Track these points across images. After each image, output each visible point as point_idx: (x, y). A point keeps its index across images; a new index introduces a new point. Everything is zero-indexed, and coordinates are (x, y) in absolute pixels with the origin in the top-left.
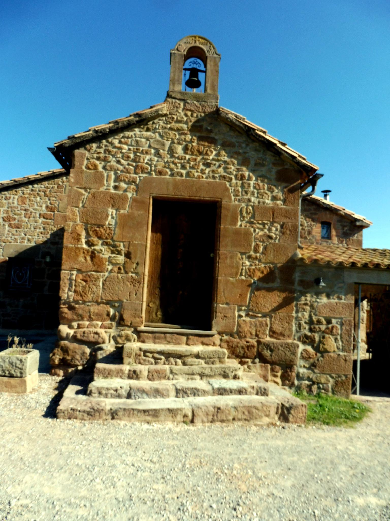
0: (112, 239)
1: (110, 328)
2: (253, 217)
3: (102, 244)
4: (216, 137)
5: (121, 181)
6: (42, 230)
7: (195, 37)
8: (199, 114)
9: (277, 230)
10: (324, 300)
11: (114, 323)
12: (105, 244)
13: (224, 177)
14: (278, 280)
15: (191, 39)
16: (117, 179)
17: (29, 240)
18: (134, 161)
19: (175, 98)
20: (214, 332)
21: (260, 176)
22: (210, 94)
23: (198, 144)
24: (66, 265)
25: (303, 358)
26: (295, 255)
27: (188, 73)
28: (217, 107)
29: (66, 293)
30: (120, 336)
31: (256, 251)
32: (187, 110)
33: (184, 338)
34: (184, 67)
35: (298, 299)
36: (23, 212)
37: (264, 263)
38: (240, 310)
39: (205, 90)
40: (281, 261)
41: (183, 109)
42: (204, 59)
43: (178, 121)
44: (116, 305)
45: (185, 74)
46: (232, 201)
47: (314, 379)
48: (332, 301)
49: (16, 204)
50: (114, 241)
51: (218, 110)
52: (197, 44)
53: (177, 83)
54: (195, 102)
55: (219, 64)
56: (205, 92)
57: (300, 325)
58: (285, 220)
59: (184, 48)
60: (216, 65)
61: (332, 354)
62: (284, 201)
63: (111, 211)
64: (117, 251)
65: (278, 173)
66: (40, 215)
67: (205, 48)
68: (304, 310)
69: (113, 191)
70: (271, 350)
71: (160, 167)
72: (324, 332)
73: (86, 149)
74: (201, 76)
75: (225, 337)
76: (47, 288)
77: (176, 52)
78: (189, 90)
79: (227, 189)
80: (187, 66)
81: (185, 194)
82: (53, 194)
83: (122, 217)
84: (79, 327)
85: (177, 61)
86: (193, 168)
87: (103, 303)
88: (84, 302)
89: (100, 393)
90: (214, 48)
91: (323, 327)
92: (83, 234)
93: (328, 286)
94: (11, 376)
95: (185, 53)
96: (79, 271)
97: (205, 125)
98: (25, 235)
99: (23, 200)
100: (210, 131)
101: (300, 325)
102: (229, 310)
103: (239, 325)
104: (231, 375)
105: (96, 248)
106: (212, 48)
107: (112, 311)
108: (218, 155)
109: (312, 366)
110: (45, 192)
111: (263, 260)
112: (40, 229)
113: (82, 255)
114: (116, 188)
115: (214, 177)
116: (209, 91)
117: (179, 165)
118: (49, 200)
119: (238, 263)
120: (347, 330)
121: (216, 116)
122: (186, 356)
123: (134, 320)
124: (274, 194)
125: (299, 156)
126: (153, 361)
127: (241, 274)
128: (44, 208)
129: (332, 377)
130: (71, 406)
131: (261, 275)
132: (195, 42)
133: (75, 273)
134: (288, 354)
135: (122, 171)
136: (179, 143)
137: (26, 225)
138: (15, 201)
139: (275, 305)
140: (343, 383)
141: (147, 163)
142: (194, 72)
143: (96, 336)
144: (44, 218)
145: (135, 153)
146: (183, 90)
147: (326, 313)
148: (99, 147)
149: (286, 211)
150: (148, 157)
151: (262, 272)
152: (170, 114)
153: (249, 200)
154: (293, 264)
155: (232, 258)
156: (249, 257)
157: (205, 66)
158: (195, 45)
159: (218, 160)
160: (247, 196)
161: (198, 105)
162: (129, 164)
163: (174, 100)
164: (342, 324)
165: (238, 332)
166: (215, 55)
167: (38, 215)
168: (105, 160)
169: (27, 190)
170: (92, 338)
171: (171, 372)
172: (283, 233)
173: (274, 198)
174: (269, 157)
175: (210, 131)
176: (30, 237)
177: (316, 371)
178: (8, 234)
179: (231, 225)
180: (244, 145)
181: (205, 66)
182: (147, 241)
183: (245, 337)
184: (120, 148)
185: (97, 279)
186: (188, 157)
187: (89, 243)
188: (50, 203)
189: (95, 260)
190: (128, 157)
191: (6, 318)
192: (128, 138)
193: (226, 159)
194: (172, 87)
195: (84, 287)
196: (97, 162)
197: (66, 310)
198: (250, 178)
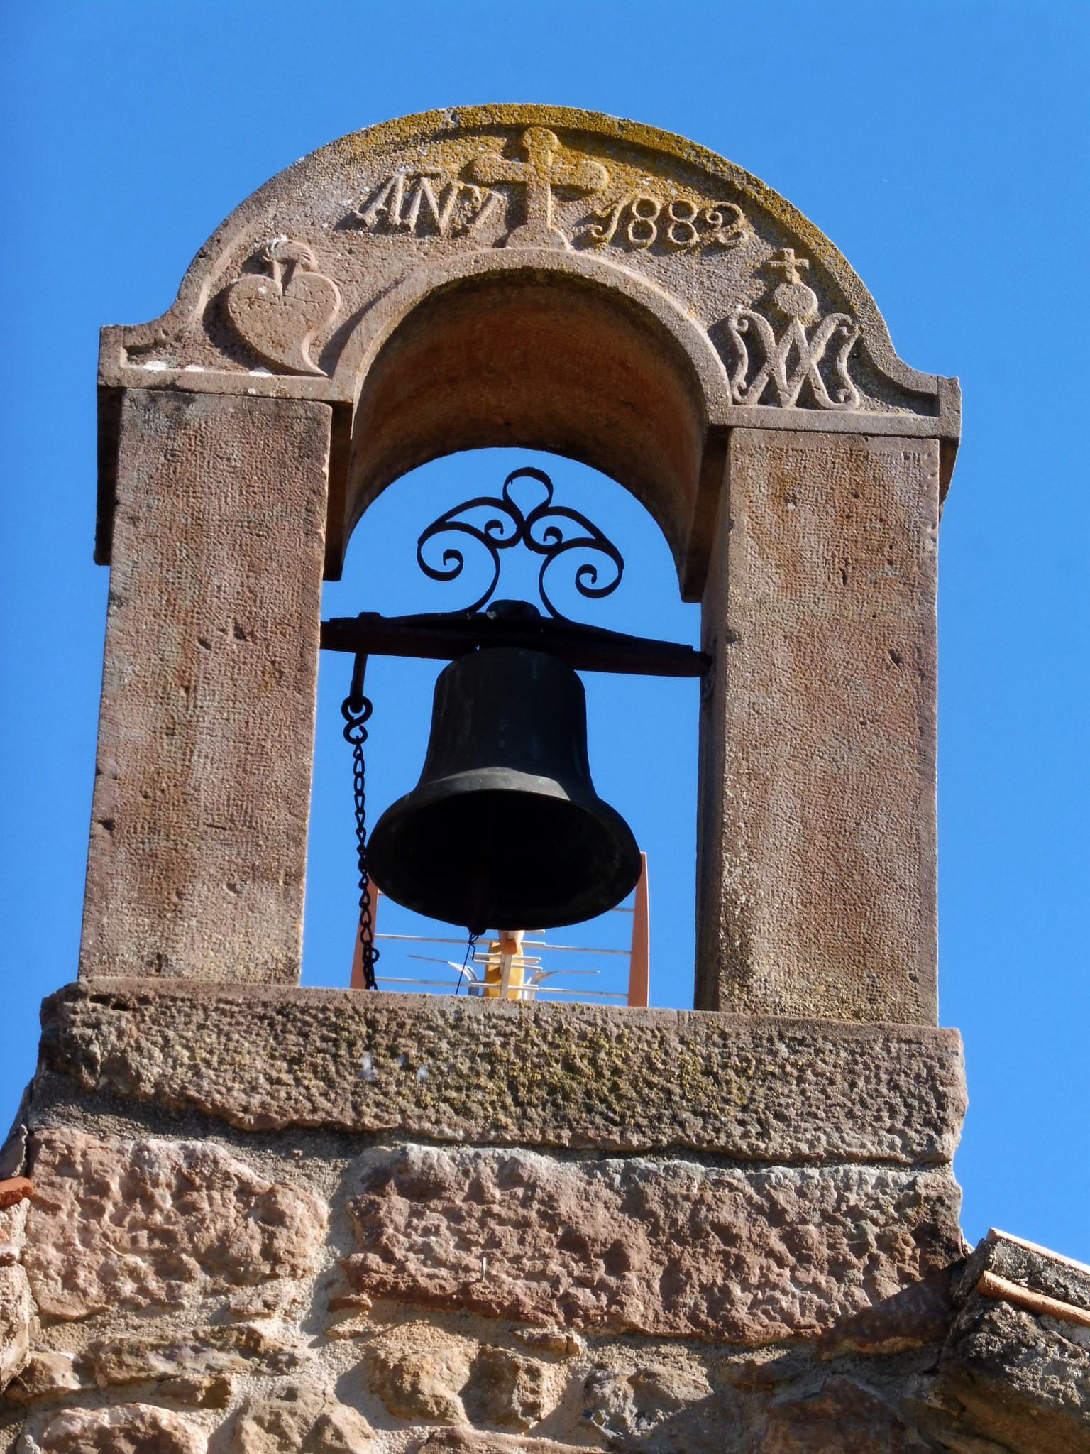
7: (515, 139)
8: (622, 1364)
15: (447, 161)
22: (801, 1034)
27: (407, 689)
28: (930, 1236)
32: (409, 1302)
34: (339, 601)
39: (716, 966)
42: (683, 477)
45: (356, 704)
51: (953, 1288)
52: (553, 242)
53: (213, 856)
54: (540, 1165)
55: (934, 542)
56: (706, 996)
59: (335, 306)
60: (880, 552)
67: (682, 299)
74: (635, 743)
77: (204, 369)
78: (427, 958)
80: (388, 571)
85: (225, 504)
90: (833, 299)
95: (352, 384)
106: (802, 301)
116: (776, 969)
121: (923, 1390)
130: (470, 1320)
132: (517, 216)
142: (514, 674)
146: (326, 977)
152: (97, 1376)
157: (700, 574)
158: (524, 252)
161: (602, 1223)
163: (165, 1149)
166: (860, 408)
181: (700, 574)
194: (127, 929)
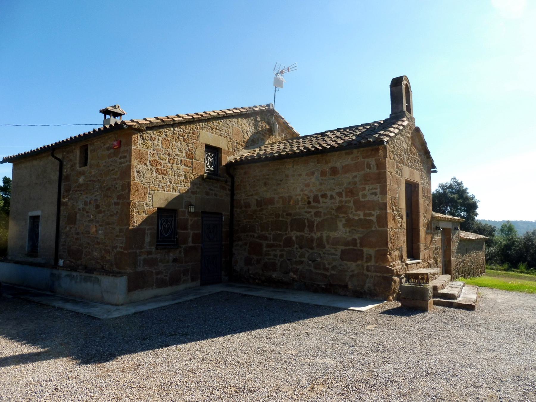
17: (174, 188)
36: (168, 157)
66: (181, 161)
76: (190, 239)
82: (191, 140)
98: (171, 182)
110: (184, 137)
118: (188, 146)
128: (184, 155)
137: (171, 171)
138: (160, 144)
167: (179, 162)
169: (169, 132)
176: (174, 185)
188: (189, 150)
191: (159, 277)
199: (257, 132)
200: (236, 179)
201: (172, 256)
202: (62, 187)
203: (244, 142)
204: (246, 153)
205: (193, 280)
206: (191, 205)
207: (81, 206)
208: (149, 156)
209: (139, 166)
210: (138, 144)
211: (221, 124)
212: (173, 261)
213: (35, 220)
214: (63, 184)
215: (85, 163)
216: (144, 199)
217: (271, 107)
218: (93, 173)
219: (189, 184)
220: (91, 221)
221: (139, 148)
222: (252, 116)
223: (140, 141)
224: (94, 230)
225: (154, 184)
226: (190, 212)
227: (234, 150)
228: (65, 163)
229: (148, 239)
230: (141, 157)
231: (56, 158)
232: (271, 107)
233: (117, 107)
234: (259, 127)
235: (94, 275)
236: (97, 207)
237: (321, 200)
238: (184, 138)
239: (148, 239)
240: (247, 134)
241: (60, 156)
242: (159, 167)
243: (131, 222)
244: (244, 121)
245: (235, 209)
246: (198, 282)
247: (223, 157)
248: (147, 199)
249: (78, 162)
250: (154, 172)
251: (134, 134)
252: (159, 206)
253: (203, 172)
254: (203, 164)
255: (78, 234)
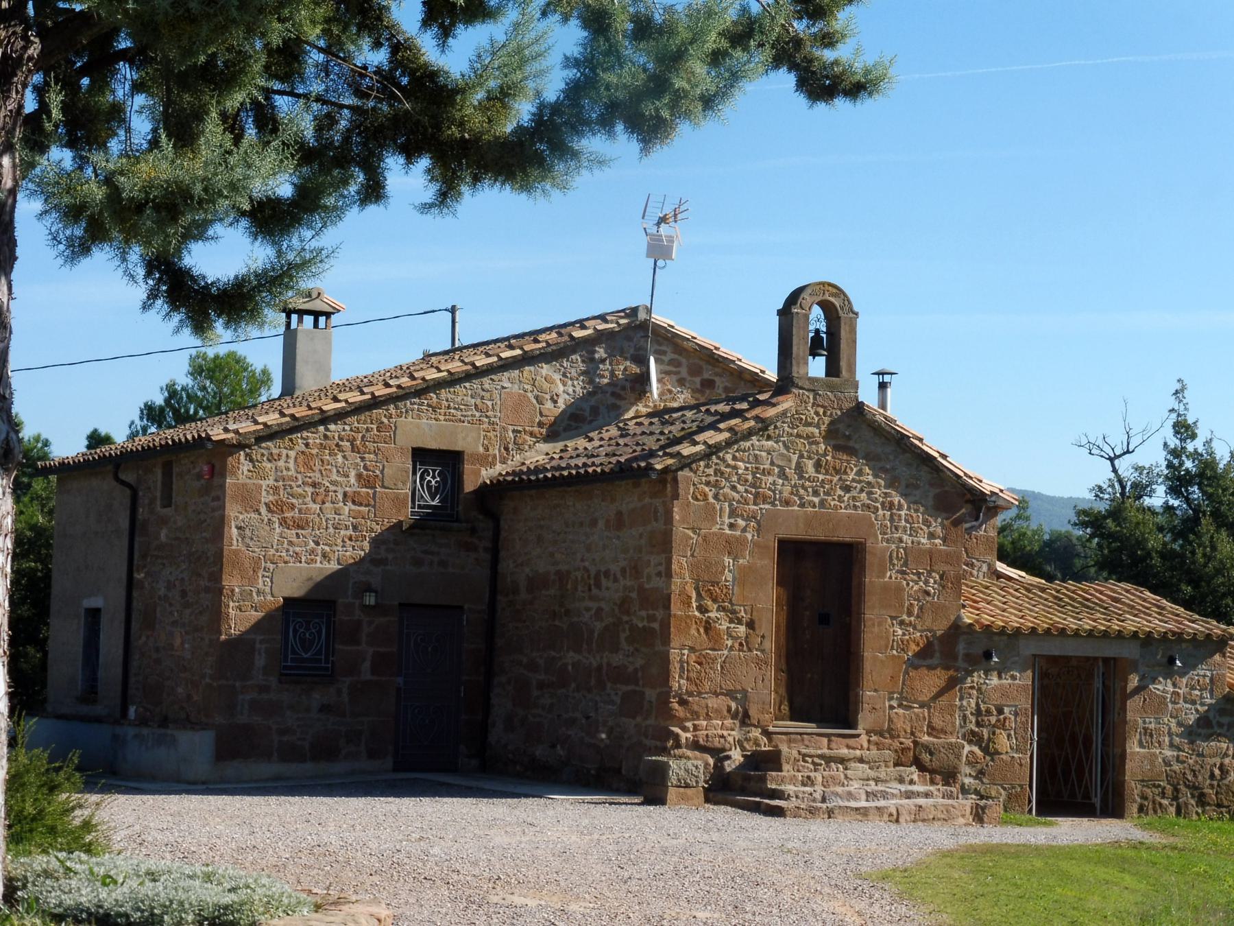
0: (731, 602)
1: (733, 730)
2: (906, 564)
3: (718, 610)
4: (857, 446)
5: (738, 516)
6: (350, 532)
9: (935, 582)
10: (994, 681)
11: (737, 722)
12: (721, 609)
13: (868, 507)
14: (937, 655)
16: (733, 513)
17: (324, 555)
18: (753, 486)
19: (802, 388)
20: (860, 731)
21: (915, 503)
23: (833, 457)
24: (675, 642)
25: (969, 763)
26: (959, 618)
29: (678, 683)
30: (747, 740)
31: (910, 614)
33: (825, 740)
35: (963, 680)
36: (310, 490)
37: (922, 631)
38: (891, 699)
40: (941, 628)
41: (813, 404)
43: (808, 424)
44: (739, 696)
46: (878, 544)
47: (983, 792)
48: (1004, 681)
49: (292, 473)
50: (732, 605)
57: (965, 717)
58: (946, 568)
61: (1004, 757)
62: (944, 540)
63: (727, 560)
64: (738, 618)
65: (937, 497)
66: (345, 495)
68: (970, 696)
69: (728, 532)
70: (931, 754)
71: (786, 494)
72: (994, 726)
73: (691, 469)
75: (874, 738)
76: (367, 665)
79: (872, 525)
81: (819, 535)
82: (370, 446)
83: (742, 569)
84: (696, 728)
86: (827, 493)
87: (722, 694)
88: (700, 693)
89: (797, 797)
91: (993, 720)
92: (694, 595)
93: (1002, 662)
94: (687, 786)
96: (692, 649)
97: (841, 426)
98: (317, 544)
99: (306, 460)
100: (849, 438)
101: (965, 717)
102: (875, 698)
103: (890, 720)
104: (907, 779)
105: (712, 615)
107: (733, 705)
108: (860, 473)
109: (980, 775)
110: (352, 442)
111: (919, 627)
112: (347, 528)
113: (694, 626)
114: (731, 526)
115: (855, 507)
117: (810, 490)
118: (363, 459)
119: (887, 631)
120: (1022, 723)
122: (849, 760)
123: (761, 717)
124: (932, 529)
125: (966, 474)
126: (811, 767)
127: (892, 648)
128: (353, 480)
129: (1005, 789)
131: (917, 649)
133: (686, 652)
134: (952, 757)
135: (739, 502)
136: (810, 458)
137: (317, 520)
138: (291, 465)
139: (935, 690)
140: (1017, 796)
141: (770, 489)
143: (722, 740)
144: (354, 502)
145: (754, 474)
147: (996, 699)
148: (707, 466)
149: (948, 554)
150: (771, 479)
151: (918, 645)
153: (901, 540)
154: (957, 629)
155: (880, 624)
156: (902, 623)
159: (859, 482)
160: (897, 530)
162: (746, 491)
164: (1016, 714)
165: (890, 730)
167: (340, 497)
168: (716, 485)
169: (314, 438)
170: (717, 743)
171: (846, 777)
172: (943, 587)
173: (932, 536)
174: (924, 473)
175: (849, 438)
176: (327, 548)
177: (985, 780)
178: (280, 543)
179: (878, 577)
180: (891, 457)
182: (767, 600)
183: (899, 736)
184: (735, 468)
185: (714, 660)
186: (821, 477)
187: (702, 609)
188: (365, 468)
189: (711, 633)
190: (746, 481)
191: (285, 739)
192: (744, 451)
193: (870, 478)
195: (699, 672)
196: (707, 489)
197: (676, 706)
198: (900, 507)
199: (597, 390)
200: (502, 522)
201: (317, 697)
202: (136, 546)
203: (540, 425)
204: (538, 455)
205: (372, 755)
206: (369, 589)
207: (162, 592)
208: (264, 493)
209: (241, 517)
210: (241, 470)
211: (462, 392)
212: (320, 710)
213: (94, 615)
214: (137, 539)
215: (167, 501)
216: (252, 581)
217: (642, 316)
218: (180, 524)
219: (366, 545)
220: (175, 623)
221: (242, 479)
222: (574, 352)
223: (245, 466)
224: (178, 642)
225: (277, 551)
226: (365, 606)
227: (506, 449)
228: (141, 494)
229: (260, 661)
230: (248, 499)
231: (123, 483)
232: (642, 316)
233: (314, 295)
234: (603, 376)
235: (169, 732)
236: (184, 593)
237: (604, 582)
238: (352, 445)
239: (260, 661)
240: (555, 402)
241: (129, 477)
242: (288, 515)
243: (224, 628)
244: (545, 369)
245: (499, 597)
246: (389, 763)
247: (466, 472)
248: (260, 581)
249: (158, 494)
250: (277, 525)
251: (231, 454)
252: (289, 593)
253: (406, 514)
254: (404, 493)
255: (157, 650)
